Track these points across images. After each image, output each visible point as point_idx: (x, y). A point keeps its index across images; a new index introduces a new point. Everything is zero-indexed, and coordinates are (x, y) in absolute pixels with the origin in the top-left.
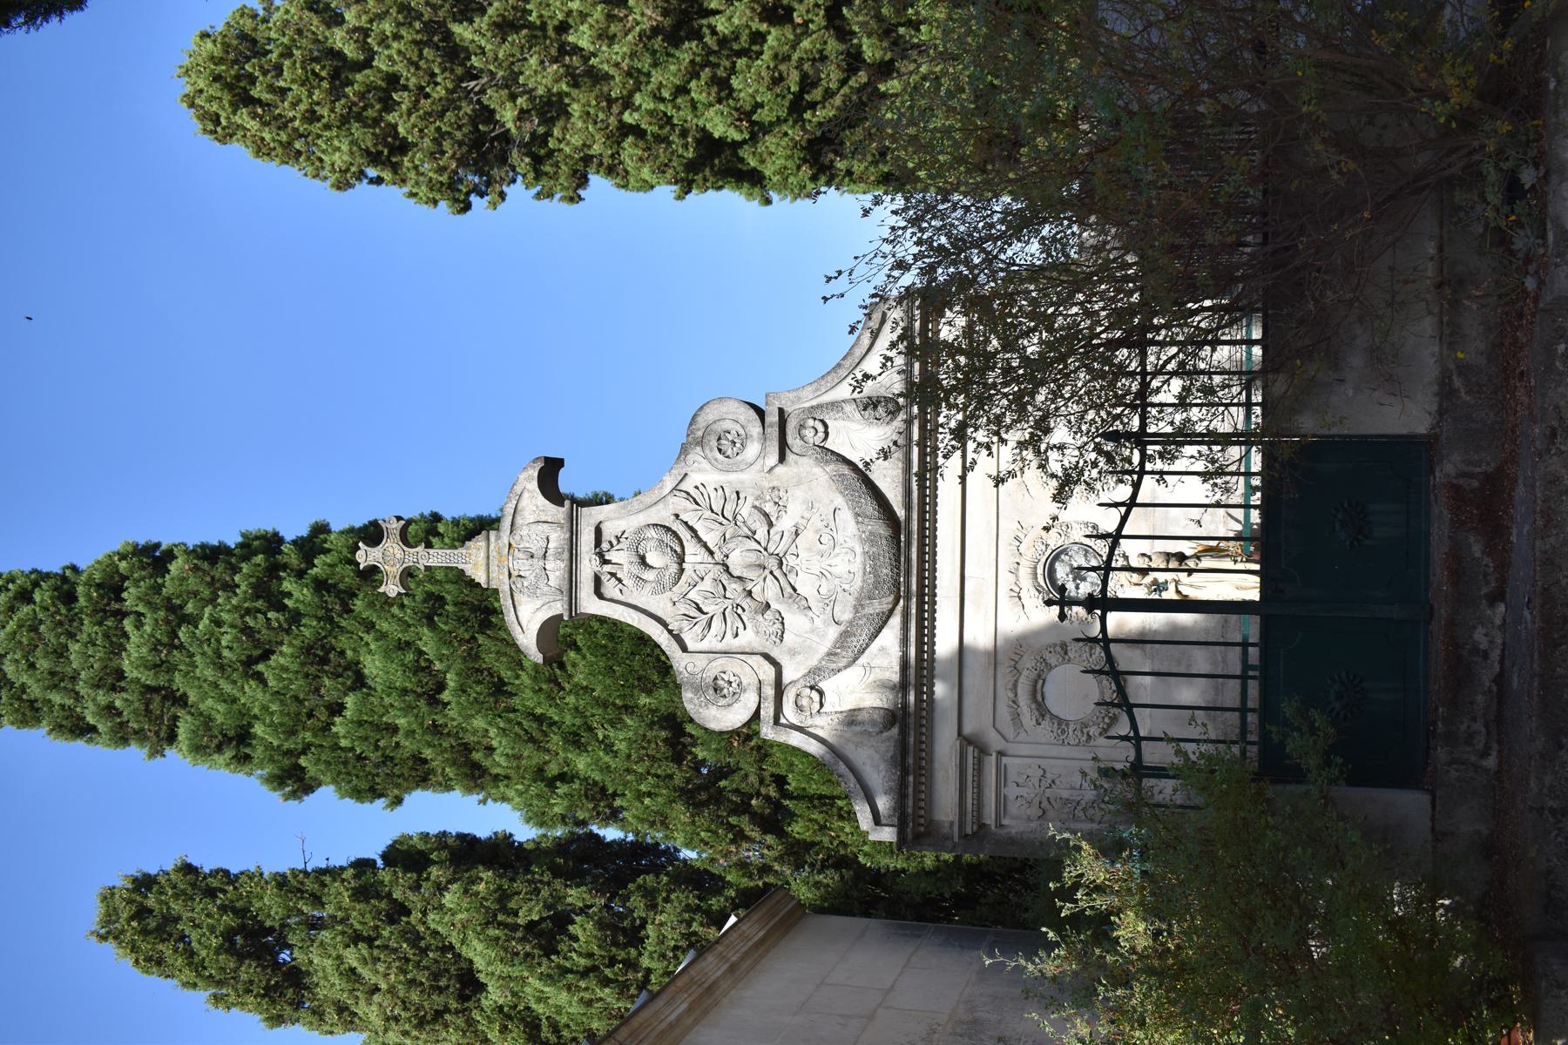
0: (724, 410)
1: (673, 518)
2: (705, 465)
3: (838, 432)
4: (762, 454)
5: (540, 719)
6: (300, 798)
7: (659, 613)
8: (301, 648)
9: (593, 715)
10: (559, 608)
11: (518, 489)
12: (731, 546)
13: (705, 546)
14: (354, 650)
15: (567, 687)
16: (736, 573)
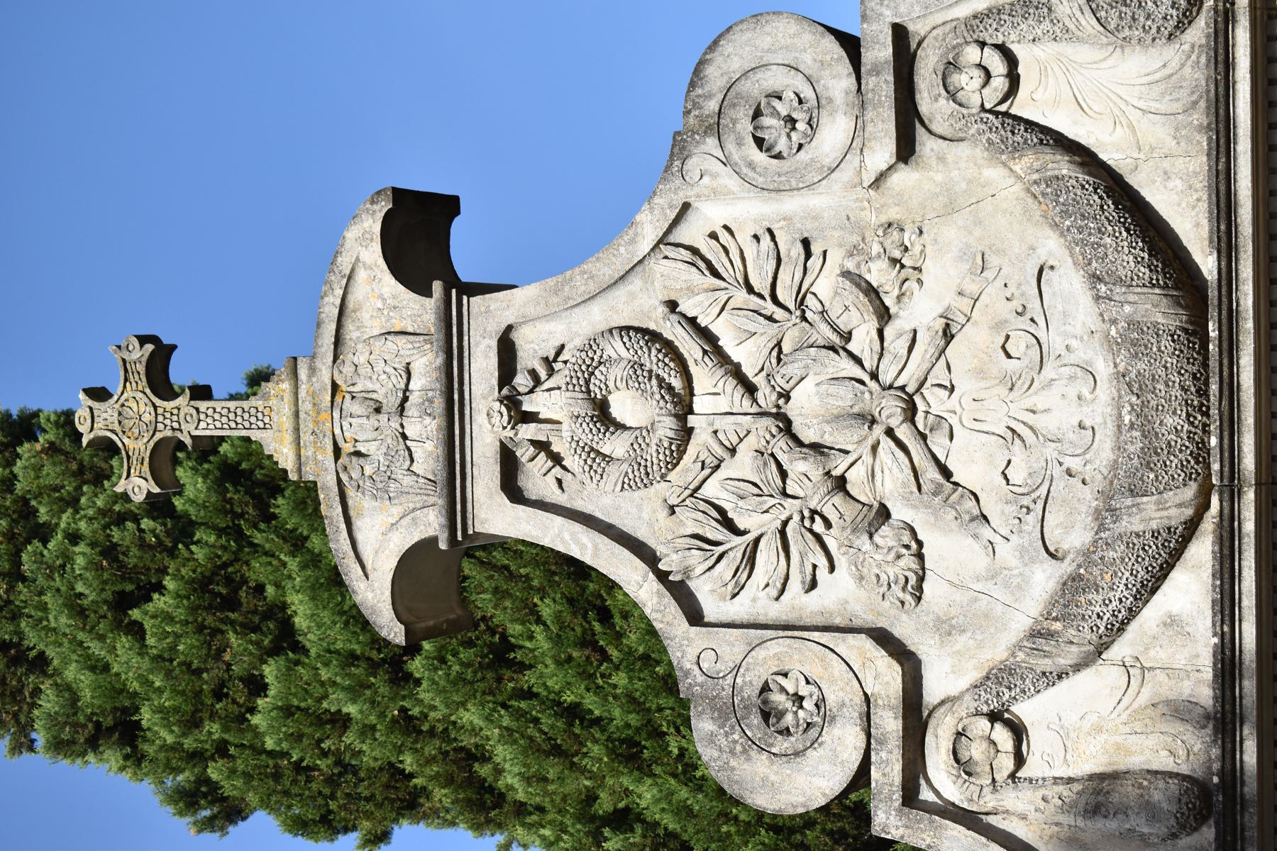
0: (766, 42)
1: (662, 310)
2: (728, 179)
3: (1043, 71)
4: (858, 142)
5: (573, 713)
6: (222, 829)
7: (642, 533)
8: (193, 581)
9: (660, 710)
10: (431, 524)
11: (344, 262)
12: (793, 369)
13: (736, 373)
14: (278, 585)
15: (614, 653)
16: (808, 436)
